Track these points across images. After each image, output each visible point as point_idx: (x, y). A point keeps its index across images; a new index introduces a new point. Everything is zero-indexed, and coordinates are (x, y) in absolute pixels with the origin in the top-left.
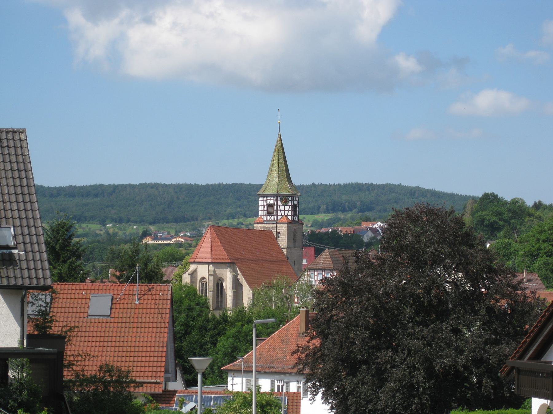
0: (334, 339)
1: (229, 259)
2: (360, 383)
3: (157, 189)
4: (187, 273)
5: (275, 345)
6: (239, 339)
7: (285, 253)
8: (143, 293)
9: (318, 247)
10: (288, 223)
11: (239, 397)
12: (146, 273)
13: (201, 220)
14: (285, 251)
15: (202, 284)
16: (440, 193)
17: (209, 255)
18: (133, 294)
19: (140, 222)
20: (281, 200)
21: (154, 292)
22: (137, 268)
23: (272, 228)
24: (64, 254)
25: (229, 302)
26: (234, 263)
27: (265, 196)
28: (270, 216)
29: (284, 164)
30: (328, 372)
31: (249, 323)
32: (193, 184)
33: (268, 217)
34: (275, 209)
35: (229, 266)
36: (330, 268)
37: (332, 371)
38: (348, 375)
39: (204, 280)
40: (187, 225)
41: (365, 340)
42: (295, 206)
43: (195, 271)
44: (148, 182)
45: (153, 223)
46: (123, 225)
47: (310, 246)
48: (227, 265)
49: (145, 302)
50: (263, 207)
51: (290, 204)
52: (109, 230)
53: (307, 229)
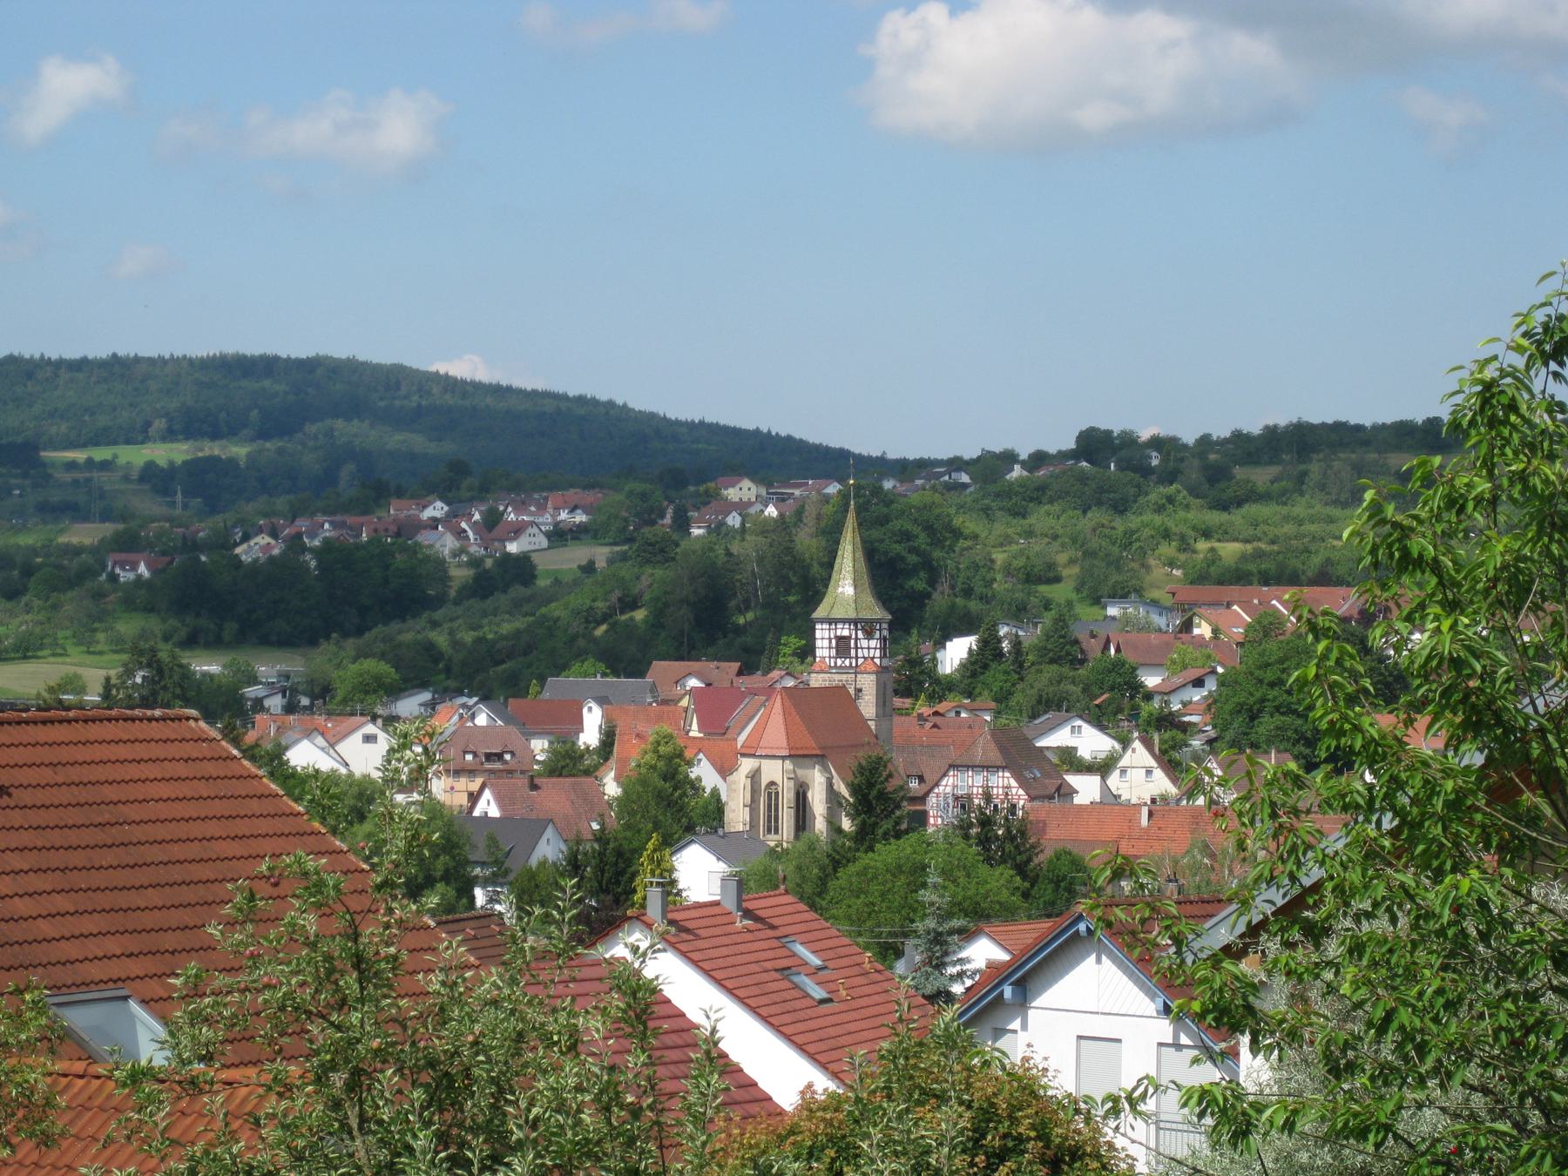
10: (877, 673)
14: (872, 725)
15: (770, 794)
16: (464, 382)
20: (863, 629)
25: (820, 825)
36: (999, 763)
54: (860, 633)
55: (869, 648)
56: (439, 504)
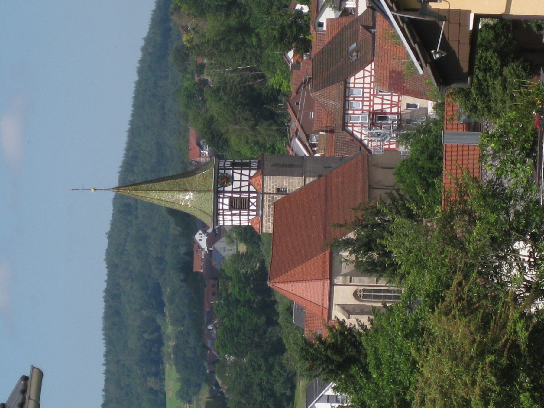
7: (311, 179)
10: (263, 175)
14: (309, 180)
15: (365, 297)
16: (126, 155)
17: (318, 285)
23: (270, 201)
24: (348, 349)
27: (216, 214)
28: (250, 204)
29: (163, 181)
33: (251, 208)
34: (238, 196)
36: (342, 87)
54: (226, 189)
55: (241, 180)
56: (197, 237)
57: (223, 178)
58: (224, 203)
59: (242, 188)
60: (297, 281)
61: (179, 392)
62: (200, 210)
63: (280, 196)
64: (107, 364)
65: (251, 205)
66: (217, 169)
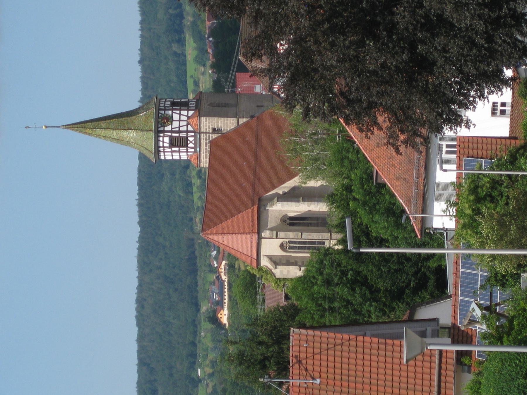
0: (377, 94)
1: (253, 206)
2: (445, 55)
3: (145, 300)
4: (274, 271)
5: (384, 156)
6: (375, 205)
7: (244, 120)
8: (304, 372)
9: (235, 68)
10: (200, 116)
11: (464, 235)
12: (274, 344)
13: (193, 233)
14: (242, 121)
15: (290, 248)
18: (306, 347)
19: (196, 326)
20: (164, 125)
21: (303, 355)
22: (266, 380)
26: (260, 200)
27: (157, 151)
28: (189, 142)
30: (427, 103)
31: (351, 188)
32: (137, 245)
33: (189, 145)
34: (177, 135)
35: (263, 208)
37: (426, 98)
38: (432, 73)
39: (285, 245)
40: (201, 254)
41: (379, 48)
42: (174, 104)
43: (271, 258)
44: (135, 313)
45: (197, 307)
46: (200, 352)
47: (235, 77)
48: (261, 210)
49: (317, 368)
50: (174, 154)
51: (170, 112)
52: (207, 374)
53: (208, 74)
57: (163, 119)
58: (164, 141)
59: (181, 128)
60: (227, 234)
61: (196, 57)
62: (143, 147)
63: (216, 135)
64: (142, 30)
65: (190, 143)
66: (158, 110)
